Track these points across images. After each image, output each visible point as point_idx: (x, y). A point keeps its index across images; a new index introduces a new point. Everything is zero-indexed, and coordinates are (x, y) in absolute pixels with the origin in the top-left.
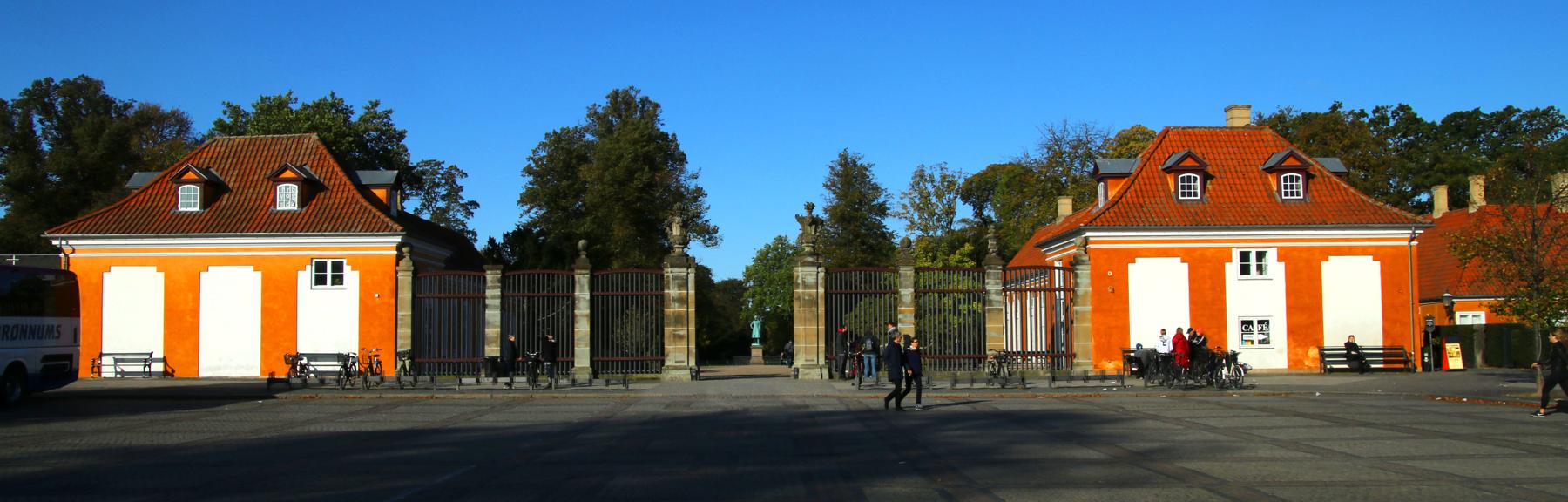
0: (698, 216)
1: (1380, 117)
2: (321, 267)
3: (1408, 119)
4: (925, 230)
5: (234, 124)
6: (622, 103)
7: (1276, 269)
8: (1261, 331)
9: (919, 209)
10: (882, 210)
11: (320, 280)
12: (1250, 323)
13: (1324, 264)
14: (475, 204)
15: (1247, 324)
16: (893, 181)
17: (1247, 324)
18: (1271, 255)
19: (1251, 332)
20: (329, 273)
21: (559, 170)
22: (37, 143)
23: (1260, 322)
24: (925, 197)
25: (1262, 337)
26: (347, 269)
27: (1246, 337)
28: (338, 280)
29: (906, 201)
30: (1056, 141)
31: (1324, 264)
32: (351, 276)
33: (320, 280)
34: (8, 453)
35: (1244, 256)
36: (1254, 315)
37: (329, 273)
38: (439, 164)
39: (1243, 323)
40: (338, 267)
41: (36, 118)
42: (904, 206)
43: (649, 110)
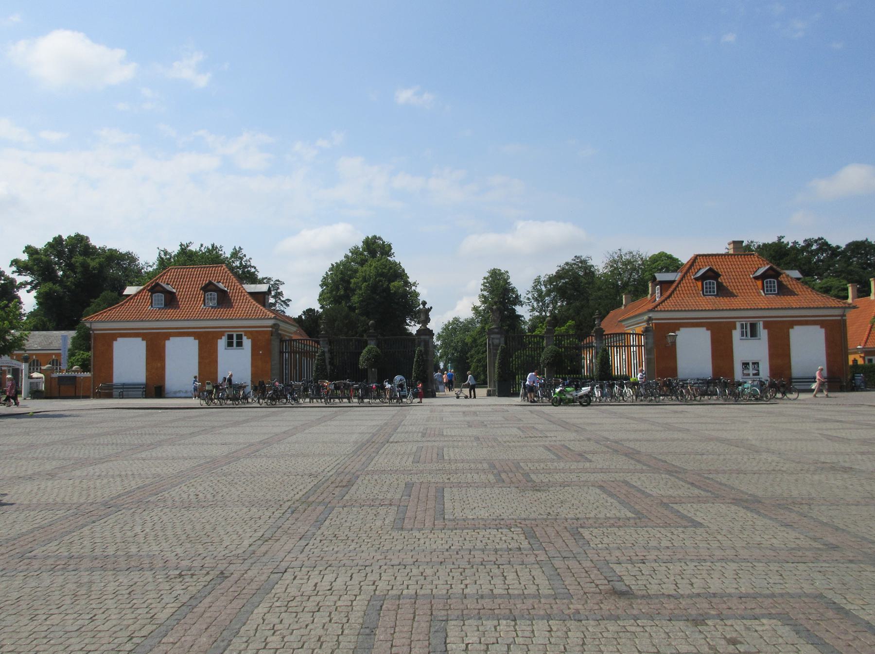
0: (140, 271)
1: (809, 243)
2: (230, 337)
3: (824, 245)
4: (540, 312)
5: (164, 263)
6: (375, 249)
7: (763, 333)
8: (754, 369)
9: (536, 300)
10: (517, 301)
11: (756, 364)
12: (748, 364)
13: (791, 330)
14: (289, 300)
15: (745, 365)
16: (522, 283)
17: (745, 365)
18: (761, 325)
19: (748, 369)
20: (235, 340)
21: (339, 283)
22: (54, 272)
23: (754, 363)
24: (540, 295)
25: (755, 372)
26: (244, 338)
27: (745, 372)
28: (240, 344)
29: (530, 296)
30: (615, 261)
31: (791, 330)
32: (247, 343)
33: (230, 344)
34: (348, 641)
35: (742, 325)
36: (750, 359)
37: (235, 340)
38: (270, 279)
39: (743, 364)
40: (239, 337)
41: (570, 323)
42: (529, 299)
43: (386, 250)
